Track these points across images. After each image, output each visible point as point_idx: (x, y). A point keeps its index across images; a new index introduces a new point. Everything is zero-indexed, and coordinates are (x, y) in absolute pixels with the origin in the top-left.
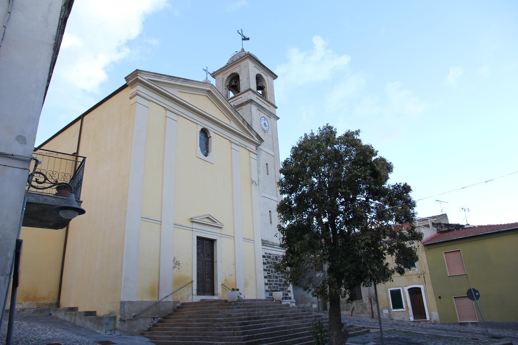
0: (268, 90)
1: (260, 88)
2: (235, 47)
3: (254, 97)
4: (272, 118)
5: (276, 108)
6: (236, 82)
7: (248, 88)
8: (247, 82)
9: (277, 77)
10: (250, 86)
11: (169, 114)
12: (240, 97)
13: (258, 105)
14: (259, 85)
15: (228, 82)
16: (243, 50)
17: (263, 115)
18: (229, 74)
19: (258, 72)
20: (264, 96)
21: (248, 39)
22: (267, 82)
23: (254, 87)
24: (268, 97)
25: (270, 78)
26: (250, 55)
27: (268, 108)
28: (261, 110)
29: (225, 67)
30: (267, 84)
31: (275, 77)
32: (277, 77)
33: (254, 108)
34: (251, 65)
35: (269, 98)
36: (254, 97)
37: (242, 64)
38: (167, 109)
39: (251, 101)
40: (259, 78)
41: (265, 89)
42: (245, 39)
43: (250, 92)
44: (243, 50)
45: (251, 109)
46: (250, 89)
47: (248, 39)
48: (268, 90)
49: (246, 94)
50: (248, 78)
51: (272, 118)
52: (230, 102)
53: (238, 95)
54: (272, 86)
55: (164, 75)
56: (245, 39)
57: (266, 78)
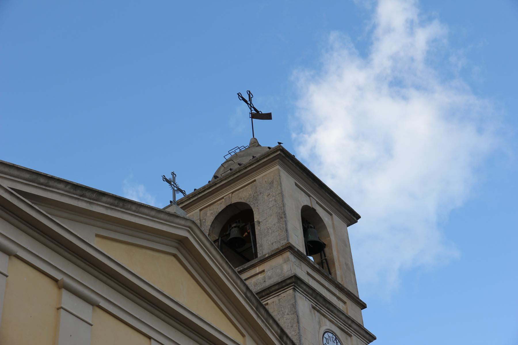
0: (334, 252)
1: (316, 246)
2: (237, 133)
3: (302, 271)
4: (354, 338)
5: (363, 306)
6: (242, 230)
7: (284, 242)
8: (277, 223)
9: (358, 217)
10: (287, 237)
11: (69, 301)
12: (258, 270)
13: (313, 295)
14: (311, 238)
15: (218, 230)
16: (255, 143)
17: (328, 325)
18: (219, 207)
19: (305, 201)
20: (325, 267)
21: (268, 116)
22: (330, 230)
23: (300, 244)
24: (338, 273)
25: (337, 220)
26: (283, 150)
27: (340, 305)
28: (324, 311)
29: (210, 185)
30: (333, 238)
31: (351, 216)
32: (358, 217)
33: (304, 305)
34: (288, 182)
35: (339, 275)
36: (302, 271)
37: (262, 177)
38: (61, 286)
39: (294, 282)
40: (309, 218)
41: (326, 250)
42: (257, 115)
43: (288, 254)
44: (255, 143)
45: (294, 306)
46: (290, 248)
47: (268, 116)
48: (335, 254)
49: (278, 260)
50: (282, 216)
51: (354, 338)
52: (244, 276)
53: (253, 266)
54: (346, 243)
55: (59, 181)
56: (257, 115)
57: (329, 220)
